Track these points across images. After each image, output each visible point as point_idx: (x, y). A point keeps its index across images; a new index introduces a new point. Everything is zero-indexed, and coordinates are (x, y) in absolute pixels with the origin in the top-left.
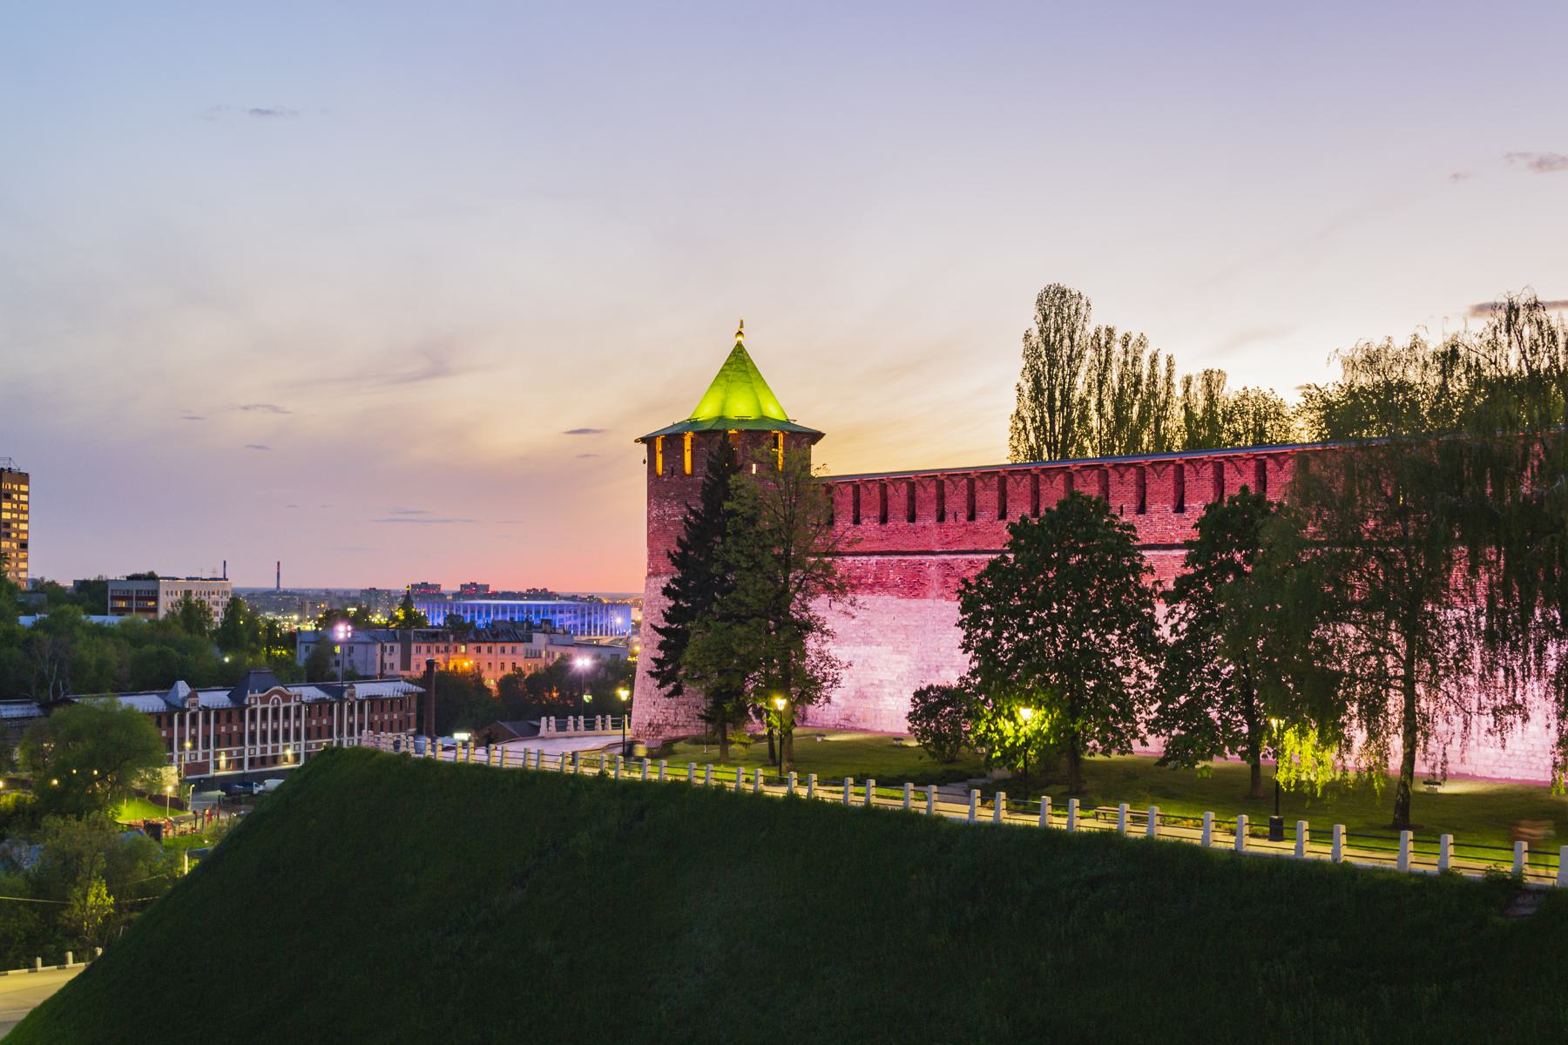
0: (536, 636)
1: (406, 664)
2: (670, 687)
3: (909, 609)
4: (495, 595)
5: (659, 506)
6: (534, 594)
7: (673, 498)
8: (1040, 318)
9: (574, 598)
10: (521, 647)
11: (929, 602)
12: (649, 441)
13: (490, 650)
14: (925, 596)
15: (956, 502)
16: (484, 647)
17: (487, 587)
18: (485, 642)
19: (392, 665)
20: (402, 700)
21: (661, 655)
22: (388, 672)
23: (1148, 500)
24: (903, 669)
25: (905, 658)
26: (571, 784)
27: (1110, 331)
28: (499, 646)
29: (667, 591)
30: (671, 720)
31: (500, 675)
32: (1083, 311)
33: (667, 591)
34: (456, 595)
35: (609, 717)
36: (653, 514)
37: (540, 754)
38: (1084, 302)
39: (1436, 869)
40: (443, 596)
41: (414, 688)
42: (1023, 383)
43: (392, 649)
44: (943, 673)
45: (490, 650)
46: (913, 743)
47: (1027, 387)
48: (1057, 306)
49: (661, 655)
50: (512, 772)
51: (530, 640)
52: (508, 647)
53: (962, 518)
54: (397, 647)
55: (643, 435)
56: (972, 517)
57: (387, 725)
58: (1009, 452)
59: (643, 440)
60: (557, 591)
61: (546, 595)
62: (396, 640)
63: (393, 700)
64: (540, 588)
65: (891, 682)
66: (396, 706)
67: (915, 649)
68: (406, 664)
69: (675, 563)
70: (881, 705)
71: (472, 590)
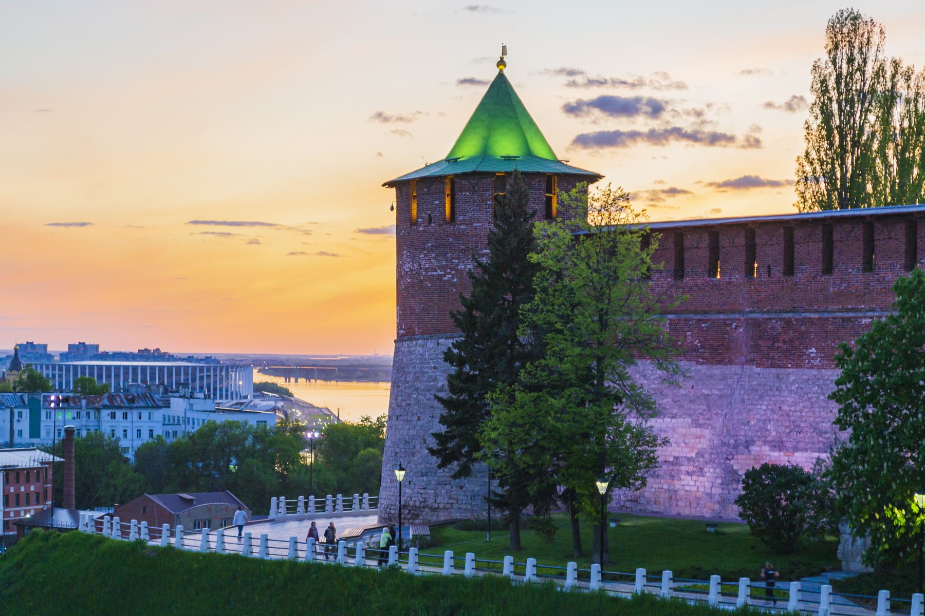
0: (173, 401)
1: (35, 431)
2: (455, 466)
3: (711, 377)
4: (105, 356)
5: (413, 258)
6: (144, 354)
7: (430, 250)
8: (831, 46)
9: (190, 358)
10: (158, 414)
11: (736, 369)
12: (400, 185)
13: (125, 416)
14: (731, 362)
15: (697, 253)
16: (119, 414)
17: (45, 346)
18: (120, 408)
19: (20, 432)
20: (38, 470)
21: (443, 429)
22: (17, 439)
23: (836, 256)
24: (703, 444)
25: (707, 432)
26: (356, 579)
27: (896, 64)
28: (135, 413)
29: (449, 357)
30: (430, 501)
31: (138, 443)
32: (875, 39)
33: (449, 357)
34: (63, 356)
35: (312, 497)
36: (407, 267)
37: (266, 539)
38: (877, 29)
39: (286, 552)
40: (50, 357)
41: (49, 457)
42: (812, 120)
43: (20, 414)
44: (755, 449)
45: (125, 416)
46: (507, 512)
47: (815, 124)
48: (848, 31)
49: (443, 429)
50: (280, 563)
51: (168, 405)
52: (145, 414)
53: (778, 271)
54: (26, 413)
55: (394, 177)
56: (790, 270)
57: (23, 498)
58: (796, 198)
59: (391, 184)
60: (171, 351)
61: (158, 355)
62: (24, 406)
63: (29, 470)
64: (152, 348)
65: (689, 460)
66: (33, 477)
67: (719, 422)
68: (35, 431)
69: (458, 323)
70: (677, 485)
71: (79, 350)
